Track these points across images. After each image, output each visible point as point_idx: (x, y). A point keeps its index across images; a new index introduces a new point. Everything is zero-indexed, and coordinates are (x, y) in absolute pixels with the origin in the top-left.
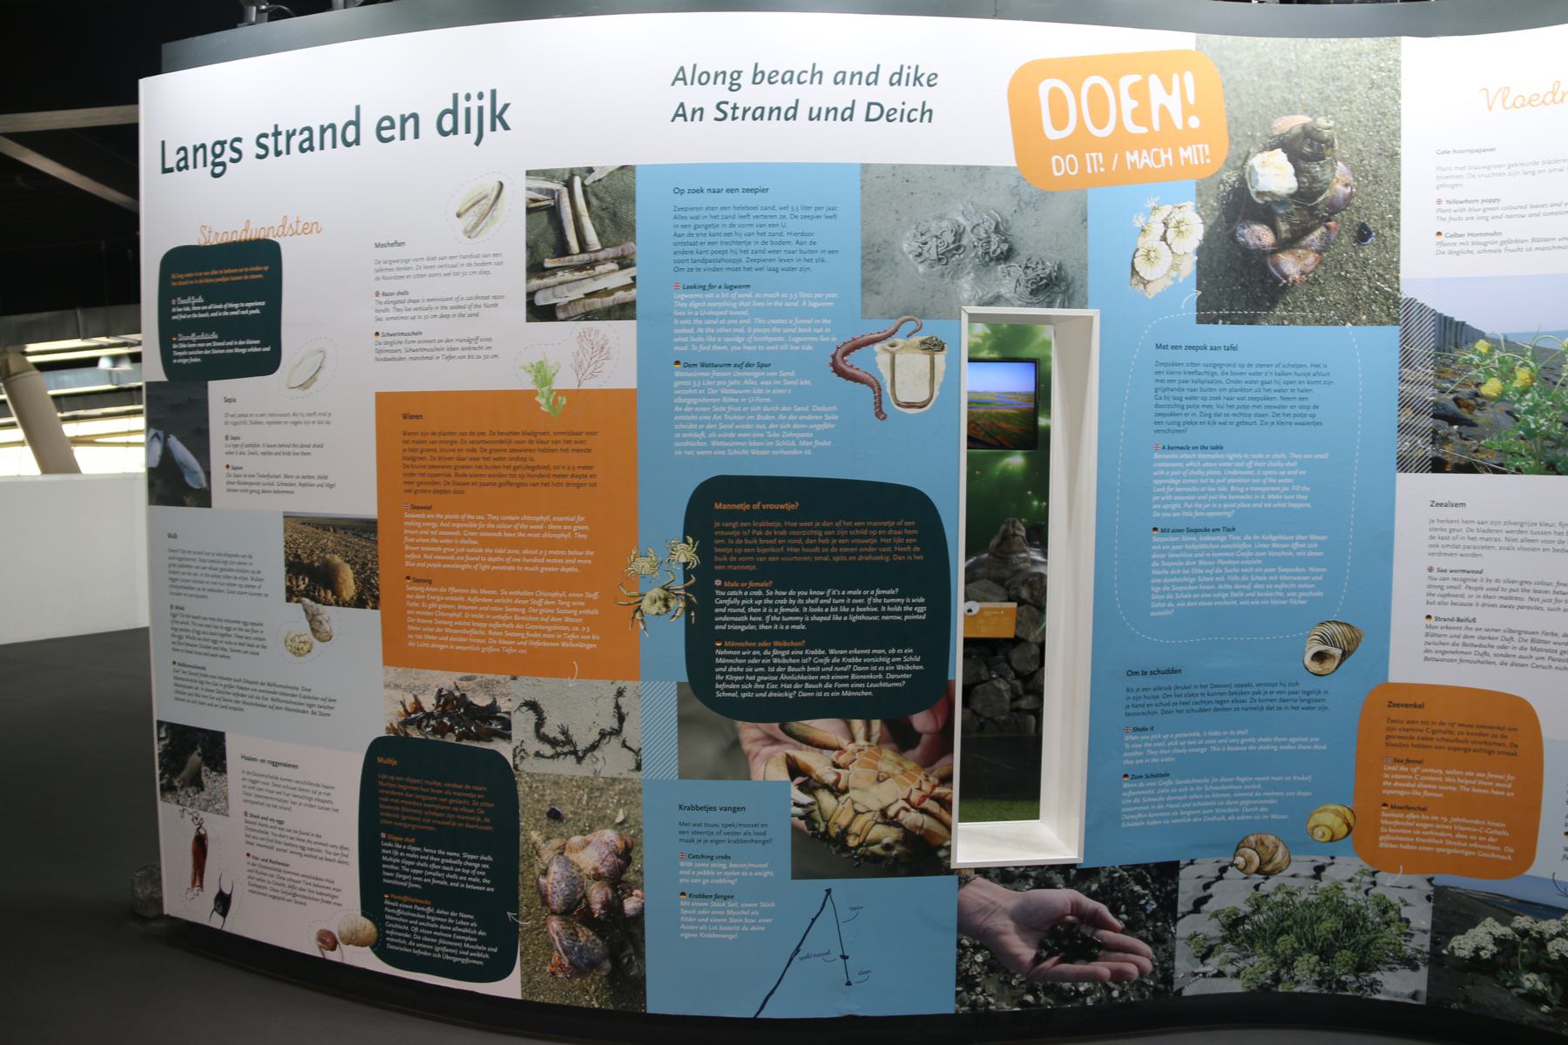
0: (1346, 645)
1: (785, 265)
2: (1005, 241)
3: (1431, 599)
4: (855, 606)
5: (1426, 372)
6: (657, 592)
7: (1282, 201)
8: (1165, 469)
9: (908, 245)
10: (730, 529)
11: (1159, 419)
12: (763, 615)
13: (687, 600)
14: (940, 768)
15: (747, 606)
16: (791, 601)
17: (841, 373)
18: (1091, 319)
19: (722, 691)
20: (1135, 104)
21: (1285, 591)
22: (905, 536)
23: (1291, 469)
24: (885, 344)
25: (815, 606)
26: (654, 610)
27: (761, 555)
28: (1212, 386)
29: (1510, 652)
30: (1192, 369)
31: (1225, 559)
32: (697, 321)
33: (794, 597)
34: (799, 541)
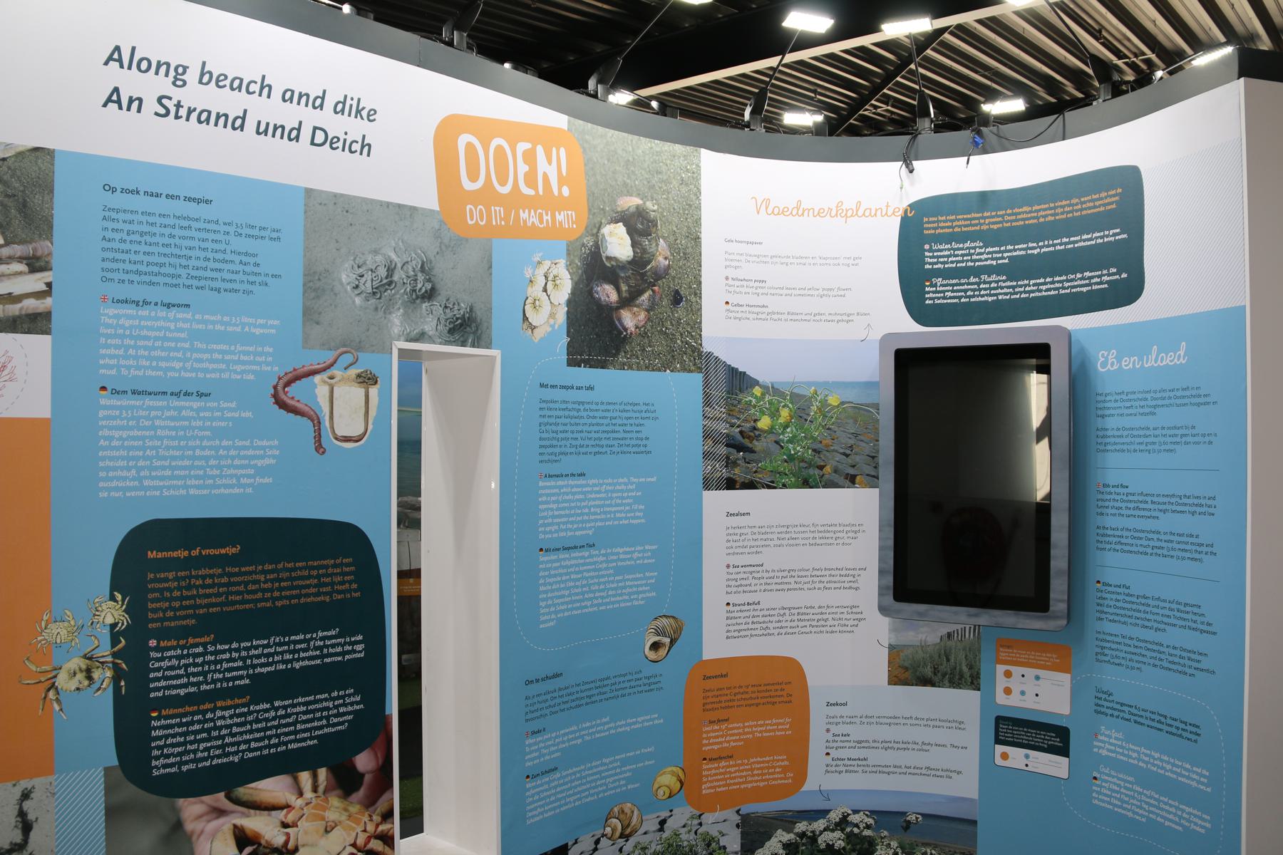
0: (673, 634)
1: (229, 286)
2: (429, 280)
3: (729, 590)
4: (298, 651)
5: (720, 411)
6: (76, 663)
7: (623, 266)
8: (547, 495)
9: (346, 276)
10: (166, 580)
11: (542, 450)
12: (204, 674)
13: (116, 667)
14: (381, 806)
15: (187, 666)
16: (235, 655)
17: (282, 405)
18: (493, 358)
19: (159, 768)
20: (526, 168)
21: (630, 594)
22: (344, 574)
23: (632, 491)
24: (324, 376)
25: (258, 657)
26: (73, 685)
27: (201, 606)
28: (577, 421)
29: (784, 624)
30: (564, 406)
31: (588, 571)
32: (127, 341)
33: (237, 650)
34: (242, 588)
